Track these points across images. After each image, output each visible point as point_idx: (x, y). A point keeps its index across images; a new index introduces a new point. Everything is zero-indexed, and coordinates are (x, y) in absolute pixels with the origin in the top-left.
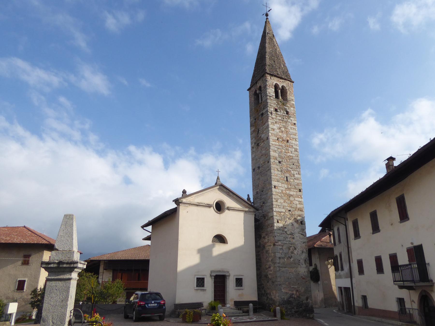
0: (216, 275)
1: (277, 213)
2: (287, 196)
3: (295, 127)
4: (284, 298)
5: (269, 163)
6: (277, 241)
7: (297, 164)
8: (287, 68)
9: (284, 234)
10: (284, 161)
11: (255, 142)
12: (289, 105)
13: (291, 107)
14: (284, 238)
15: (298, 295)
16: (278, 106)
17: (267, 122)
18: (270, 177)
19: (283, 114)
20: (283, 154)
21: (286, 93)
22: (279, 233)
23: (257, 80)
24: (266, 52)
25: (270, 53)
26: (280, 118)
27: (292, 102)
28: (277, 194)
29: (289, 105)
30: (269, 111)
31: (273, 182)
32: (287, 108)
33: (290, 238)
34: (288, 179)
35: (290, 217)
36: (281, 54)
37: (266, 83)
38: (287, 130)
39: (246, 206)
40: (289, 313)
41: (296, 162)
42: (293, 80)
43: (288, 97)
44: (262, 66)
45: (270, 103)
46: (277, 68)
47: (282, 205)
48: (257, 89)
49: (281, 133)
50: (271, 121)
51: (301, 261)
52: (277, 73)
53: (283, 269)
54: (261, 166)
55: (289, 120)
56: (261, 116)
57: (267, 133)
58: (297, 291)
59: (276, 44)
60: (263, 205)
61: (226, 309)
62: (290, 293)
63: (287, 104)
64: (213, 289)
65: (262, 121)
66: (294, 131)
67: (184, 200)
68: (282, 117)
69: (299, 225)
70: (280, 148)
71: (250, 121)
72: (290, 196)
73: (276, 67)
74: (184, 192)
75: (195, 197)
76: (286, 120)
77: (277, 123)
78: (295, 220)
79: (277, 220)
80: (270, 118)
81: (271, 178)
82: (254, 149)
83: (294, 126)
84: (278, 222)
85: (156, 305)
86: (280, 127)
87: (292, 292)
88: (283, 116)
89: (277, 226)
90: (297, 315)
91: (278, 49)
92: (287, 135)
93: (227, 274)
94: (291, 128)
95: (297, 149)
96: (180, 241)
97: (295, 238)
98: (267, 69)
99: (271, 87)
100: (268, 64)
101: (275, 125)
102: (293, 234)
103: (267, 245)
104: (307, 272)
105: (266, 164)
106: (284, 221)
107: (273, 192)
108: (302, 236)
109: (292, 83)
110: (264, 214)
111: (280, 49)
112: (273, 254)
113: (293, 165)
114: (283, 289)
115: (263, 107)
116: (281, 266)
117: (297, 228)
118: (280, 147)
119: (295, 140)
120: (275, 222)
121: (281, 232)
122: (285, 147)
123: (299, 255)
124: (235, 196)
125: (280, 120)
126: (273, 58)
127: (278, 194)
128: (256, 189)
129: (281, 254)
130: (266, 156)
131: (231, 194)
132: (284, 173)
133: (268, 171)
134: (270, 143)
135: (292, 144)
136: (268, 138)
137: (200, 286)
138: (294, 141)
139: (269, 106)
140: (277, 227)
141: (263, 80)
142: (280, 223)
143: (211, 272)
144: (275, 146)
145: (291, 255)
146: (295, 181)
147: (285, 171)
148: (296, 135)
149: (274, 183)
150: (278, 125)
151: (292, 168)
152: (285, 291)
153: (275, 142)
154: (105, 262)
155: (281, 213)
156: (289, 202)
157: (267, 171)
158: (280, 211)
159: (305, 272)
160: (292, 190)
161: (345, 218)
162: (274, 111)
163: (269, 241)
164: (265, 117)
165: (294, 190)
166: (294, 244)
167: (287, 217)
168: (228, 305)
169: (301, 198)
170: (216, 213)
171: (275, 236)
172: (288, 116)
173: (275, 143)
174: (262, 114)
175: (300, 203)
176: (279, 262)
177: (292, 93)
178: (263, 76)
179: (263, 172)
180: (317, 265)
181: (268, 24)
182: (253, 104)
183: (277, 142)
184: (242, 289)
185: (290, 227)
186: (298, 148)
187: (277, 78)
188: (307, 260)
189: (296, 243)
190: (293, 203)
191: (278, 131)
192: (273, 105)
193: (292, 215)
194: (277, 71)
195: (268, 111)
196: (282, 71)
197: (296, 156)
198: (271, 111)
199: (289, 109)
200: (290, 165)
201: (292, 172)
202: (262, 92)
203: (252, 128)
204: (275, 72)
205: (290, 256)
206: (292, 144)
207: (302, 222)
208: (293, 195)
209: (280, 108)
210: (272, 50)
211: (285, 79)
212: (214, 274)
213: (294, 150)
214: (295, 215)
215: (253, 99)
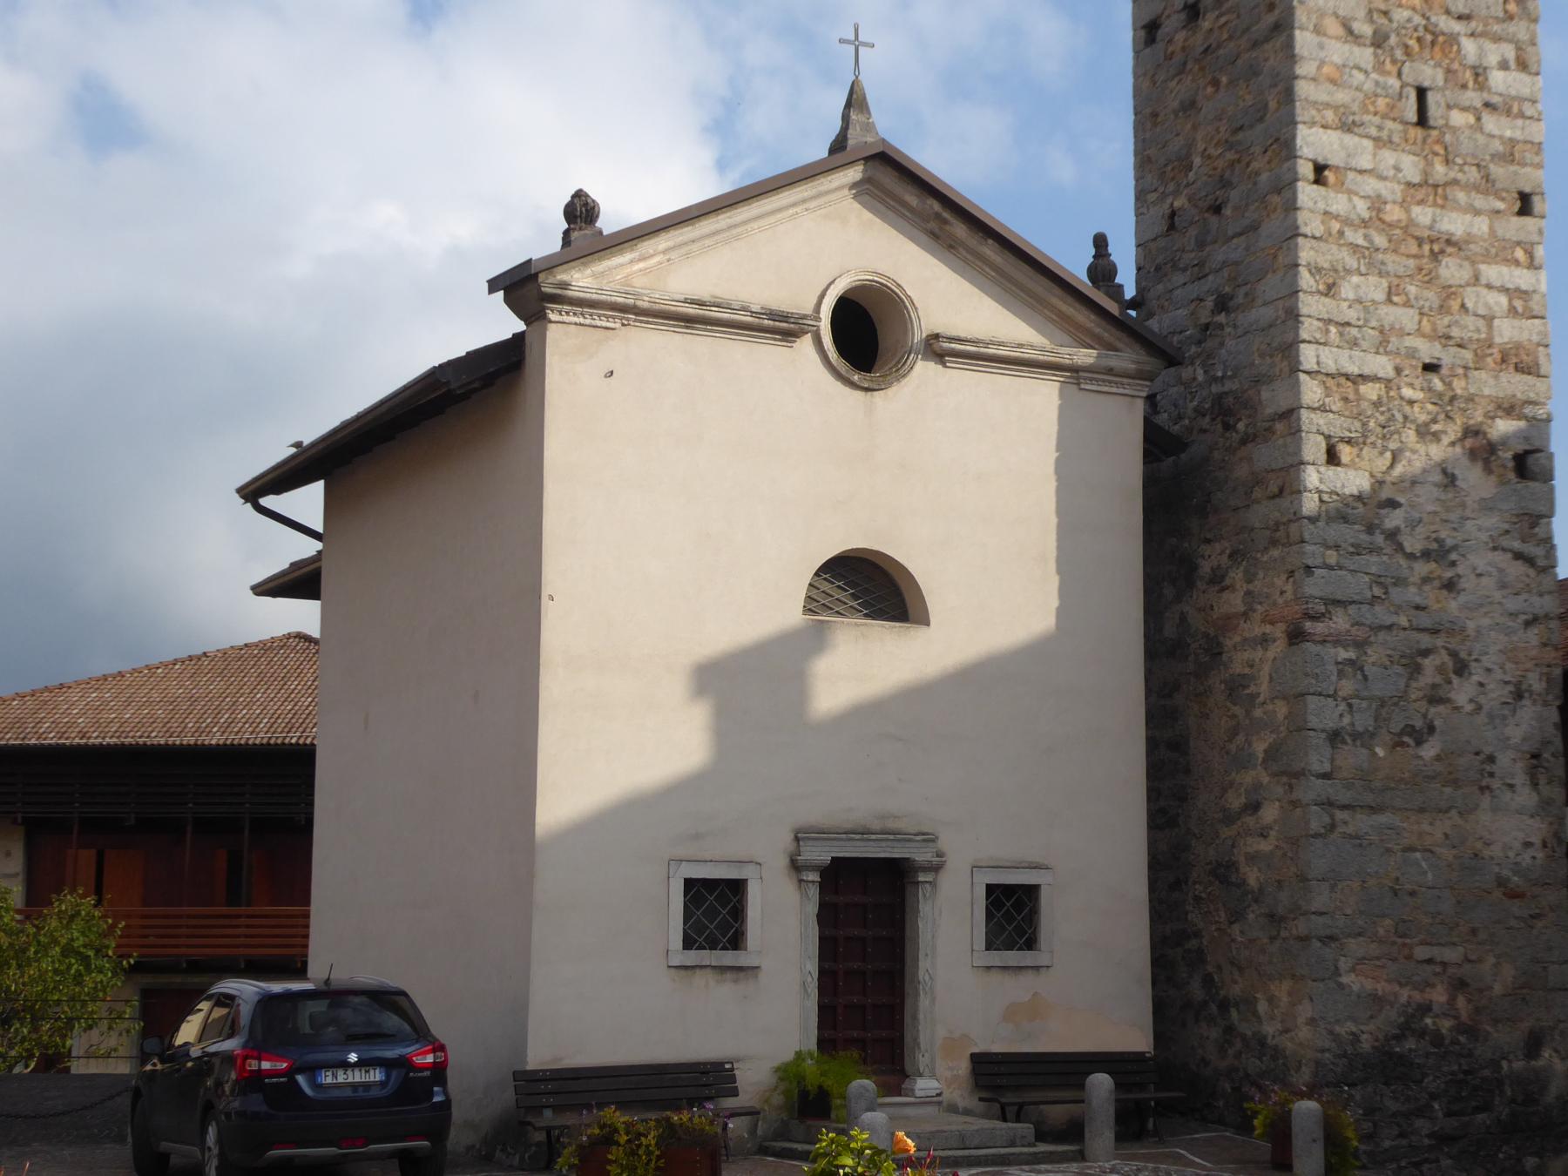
1: (1330, 382)
6: (1322, 609)
22: (1337, 547)
81: (1288, 96)
84: (1332, 458)
89: (1322, 487)
93: (921, 855)
103: (1237, 639)
124: (989, 250)
127: (1341, 233)
128: (1164, 196)
131: (960, 230)
132: (1399, 54)
133: (1267, 40)
140: (1326, 497)
143: (797, 839)
146: (1491, 123)
147: (1412, 43)
157: (1255, 45)
168: (924, 1086)
179: (1221, 52)
184: (1037, 968)
201: (1469, 47)
212: (821, 854)
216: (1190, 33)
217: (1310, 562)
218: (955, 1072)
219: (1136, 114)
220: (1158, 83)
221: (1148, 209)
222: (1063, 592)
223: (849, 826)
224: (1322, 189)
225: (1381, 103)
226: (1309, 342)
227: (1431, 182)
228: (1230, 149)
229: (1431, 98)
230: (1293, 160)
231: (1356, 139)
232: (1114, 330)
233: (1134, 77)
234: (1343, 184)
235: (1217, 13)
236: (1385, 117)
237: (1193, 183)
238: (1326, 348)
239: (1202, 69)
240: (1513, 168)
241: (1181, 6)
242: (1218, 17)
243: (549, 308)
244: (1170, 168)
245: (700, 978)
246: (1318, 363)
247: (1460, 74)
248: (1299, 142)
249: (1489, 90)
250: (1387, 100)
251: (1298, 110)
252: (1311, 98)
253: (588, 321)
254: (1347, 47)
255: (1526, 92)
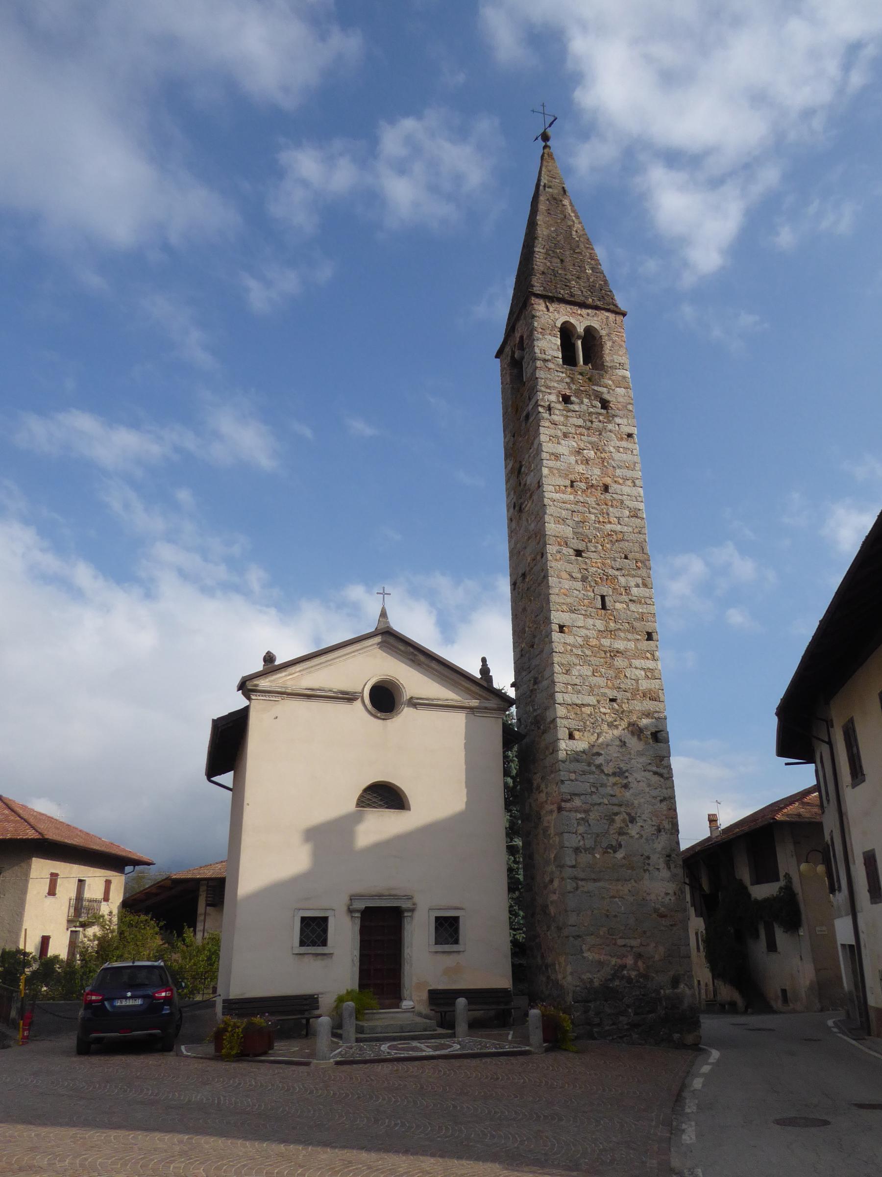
0: (366, 908)
2: (603, 655)
3: (630, 446)
4: (591, 981)
6: (569, 797)
7: (638, 556)
9: (593, 773)
10: (593, 549)
12: (610, 382)
14: (593, 785)
15: (642, 970)
16: (574, 387)
19: (592, 410)
22: (575, 772)
25: (549, 238)
27: (621, 372)
28: (568, 650)
29: (610, 382)
30: (542, 403)
31: (553, 614)
32: (605, 390)
33: (615, 787)
35: (615, 721)
37: (532, 324)
38: (602, 455)
39: (477, 693)
40: (607, 1028)
42: (622, 305)
43: (607, 358)
46: (571, 277)
47: (587, 684)
49: (584, 467)
50: (547, 433)
51: (654, 858)
52: (571, 292)
53: (590, 886)
58: (639, 956)
59: (570, 212)
60: (536, 687)
61: (398, 1015)
62: (613, 963)
63: (602, 380)
64: (357, 953)
67: (264, 683)
69: (647, 743)
70: (578, 512)
72: (616, 653)
73: (566, 275)
74: (269, 658)
75: (300, 671)
76: (601, 425)
78: (630, 729)
79: (567, 732)
81: (548, 601)
83: (627, 441)
84: (571, 737)
85: (139, 1002)
86: (580, 449)
87: (619, 961)
88: (590, 414)
89: (567, 748)
90: (635, 1036)
91: (577, 226)
93: (405, 905)
94: (618, 449)
95: (639, 510)
96: (248, 804)
97: (634, 785)
98: (536, 284)
100: (542, 269)
101: (563, 442)
102: (624, 772)
104: (675, 894)
106: (594, 732)
107: (554, 645)
108: (656, 778)
109: (619, 318)
110: (536, 716)
112: (557, 839)
114: (589, 950)
116: (582, 875)
117: (640, 754)
118: (581, 509)
119: (630, 484)
120: (560, 736)
121: (583, 766)
122: (596, 506)
123: (647, 840)
124: (434, 665)
125: (580, 427)
126: (558, 251)
127: (572, 650)
129: (583, 837)
131: (422, 658)
132: (593, 584)
134: (546, 496)
136: (540, 485)
137: (314, 944)
138: (627, 487)
139: (543, 389)
140: (569, 753)
142: (580, 739)
143: (351, 899)
145: (617, 841)
146: (633, 607)
149: (557, 617)
150: (574, 444)
151: (621, 569)
152: (597, 957)
153: (563, 493)
154: (210, 884)
155: (583, 709)
156: (611, 673)
158: (580, 703)
159: (667, 894)
160: (622, 635)
161: (827, 722)
162: (560, 402)
163: (549, 798)
164: (532, 425)
165: (630, 636)
166: (628, 804)
167: (602, 720)
168: (406, 1004)
169: (654, 659)
170: (372, 718)
171: (562, 781)
172: (607, 412)
173: (562, 495)
174: (527, 417)
175: (648, 674)
176: (574, 863)
177: (621, 346)
180: (791, 878)
181: (548, 162)
184: (458, 952)
185: (614, 752)
186: (642, 506)
187: (569, 308)
188: (673, 855)
189: (636, 802)
190: (625, 675)
191: (572, 459)
192: (556, 385)
193: (620, 714)
195: (539, 403)
196: (587, 284)
197: (636, 530)
198: (548, 403)
201: (622, 580)
205: (614, 843)
206: (620, 497)
207: (659, 735)
208: (626, 650)
209: (578, 393)
211: (597, 308)
212: (361, 905)
214: (630, 712)
217: (563, 779)
218: (421, 998)
222: (469, 795)
223: (374, 893)
226: (560, 692)
232: (486, 692)
238: (567, 694)
243: (252, 694)
245: (306, 959)
246: (563, 700)
253: (267, 699)
254: (571, 582)
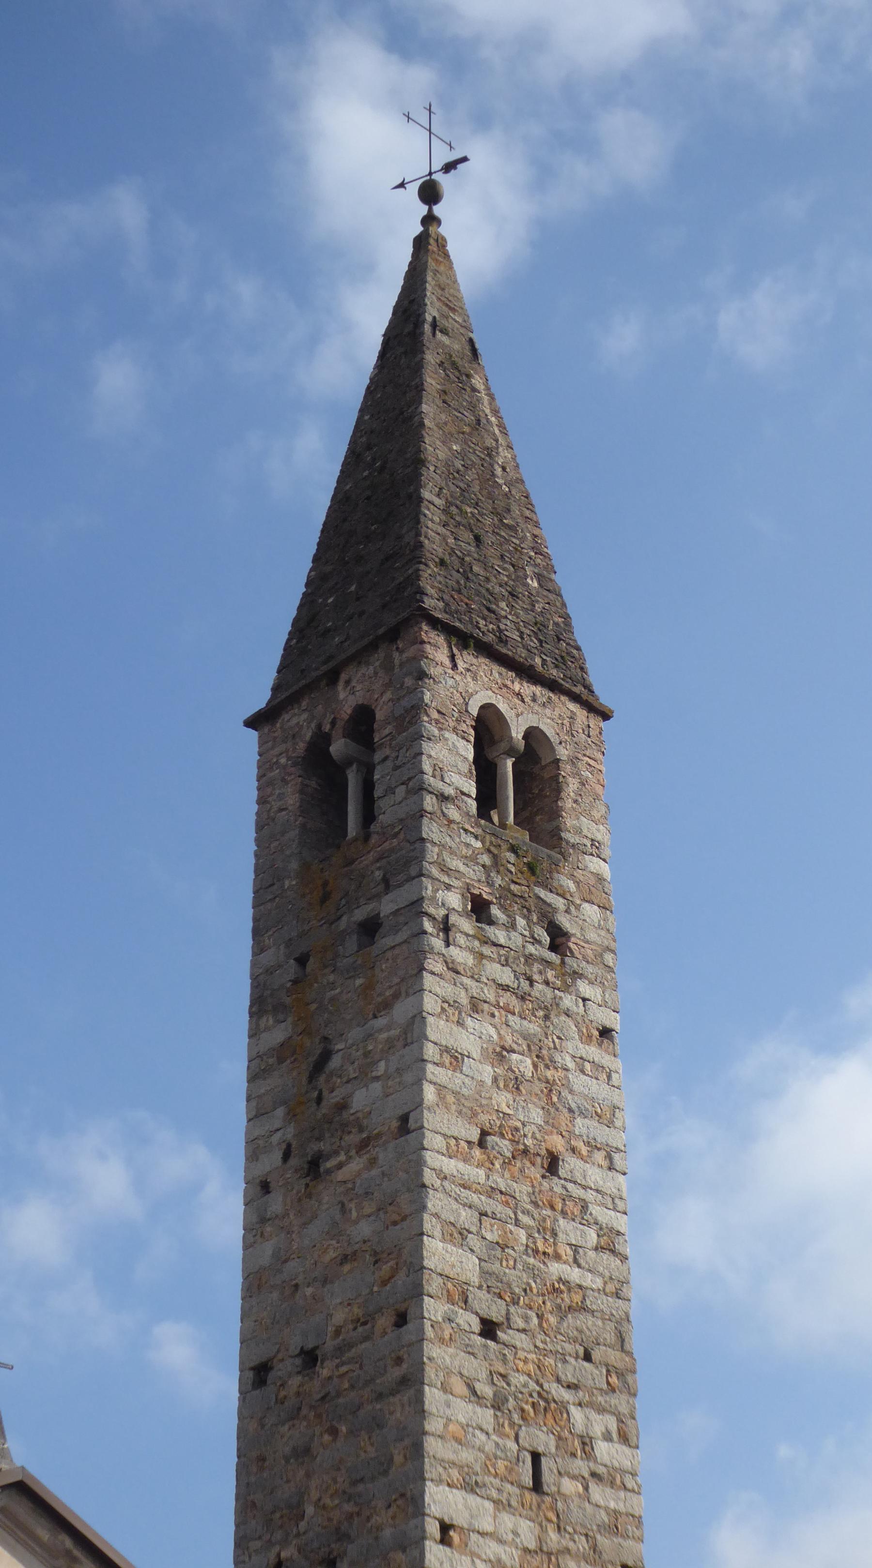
3: (606, 1060)
5: (410, 1326)
7: (614, 1357)
8: (564, 605)
10: (521, 1324)
11: (289, 1146)
13: (584, 900)
16: (498, 881)
17: (408, 995)
18: (407, 1442)
19: (531, 949)
20: (520, 1266)
21: (556, 788)
23: (343, 656)
24: (419, 462)
26: (507, 970)
27: (595, 864)
30: (432, 910)
31: (431, 1489)
32: (559, 903)
34: (548, 1477)
36: (527, 497)
37: (415, 690)
38: (549, 1074)
41: (610, 1336)
42: (605, 697)
43: (569, 821)
44: (387, 559)
45: (442, 846)
46: (497, 589)
48: (333, 723)
49: (509, 1096)
50: (438, 990)
52: (500, 631)
54: (330, 1344)
55: (568, 1001)
56: (355, 937)
57: (408, 1078)
59: (488, 411)
63: (555, 875)
65: (359, 982)
66: (597, 1088)
68: (522, 968)
71: (254, 964)
76: (549, 992)
77: (486, 1006)
80: (434, 964)
81: (417, 1451)
82: (276, 1203)
86: (503, 1048)
88: (529, 959)
91: (503, 455)
92: (552, 1110)
95: (619, 1233)
99: (455, 730)
101: (469, 1022)
105: (385, 1333)
109: (595, 722)
111: (514, 458)
113: (588, 1357)
115: (378, 874)
122: (529, 1207)
125: (506, 988)
126: (469, 510)
128: (270, 1544)
130: (386, 1268)
132: (516, 1417)
133: (393, 1393)
134: (429, 1161)
135: (585, 1188)
138: (597, 1170)
139: (435, 871)
141: (388, 666)
144: (465, 1193)
146: (597, 1492)
147: (528, 1408)
148: (610, 1124)
150: (492, 1031)
153: (465, 1161)
157: (380, 1396)
162: (468, 916)
164: (389, 954)
172: (563, 962)
173: (461, 1165)
177: (597, 798)
178: (393, 635)
179: (341, 1400)
182: (293, 834)
183: (480, 1165)
187: (496, 668)
191: (487, 1072)
192: (462, 868)
194: (493, 612)
197: (610, 1288)
198: (442, 912)
199: (567, 911)
200: (565, 1361)
201: (577, 1415)
202: (378, 757)
203: (267, 1029)
204: (482, 623)
209: (505, 895)
210: (462, 455)
211: (553, 686)
213: (594, 1236)
215: (292, 800)
216: (306, 1378)
219: (239, 1457)
220: (266, 1427)
221: (250, 1557)
224: (448, 1549)
225: (501, 1465)
227: (545, 1549)
228: (349, 1500)
229: (546, 1464)
230: (420, 1518)
231: (478, 1499)
233: (239, 1418)
234: (466, 1545)
235: (337, 1361)
236: (504, 1479)
237: (304, 1533)
239: (319, 1416)
240: (617, 1540)
241: (297, 1351)
242: (337, 1366)
244: (278, 1515)
247: (570, 1443)
248: (427, 1499)
249: (595, 1461)
250: (506, 1463)
251: (427, 1467)
252: (438, 1456)
254: (470, 1406)
255: (627, 1464)
